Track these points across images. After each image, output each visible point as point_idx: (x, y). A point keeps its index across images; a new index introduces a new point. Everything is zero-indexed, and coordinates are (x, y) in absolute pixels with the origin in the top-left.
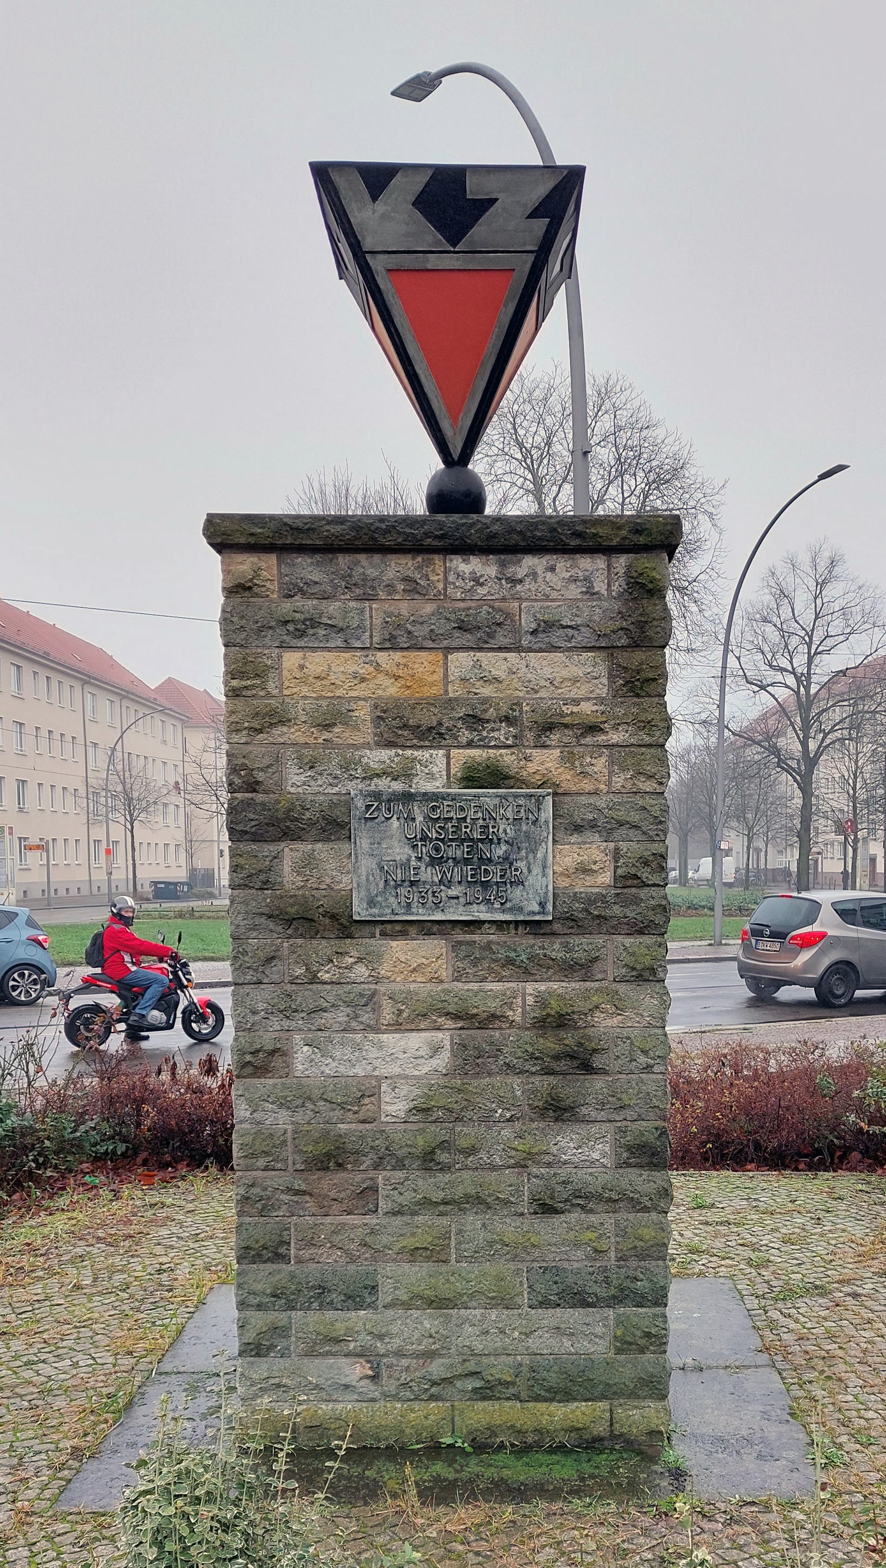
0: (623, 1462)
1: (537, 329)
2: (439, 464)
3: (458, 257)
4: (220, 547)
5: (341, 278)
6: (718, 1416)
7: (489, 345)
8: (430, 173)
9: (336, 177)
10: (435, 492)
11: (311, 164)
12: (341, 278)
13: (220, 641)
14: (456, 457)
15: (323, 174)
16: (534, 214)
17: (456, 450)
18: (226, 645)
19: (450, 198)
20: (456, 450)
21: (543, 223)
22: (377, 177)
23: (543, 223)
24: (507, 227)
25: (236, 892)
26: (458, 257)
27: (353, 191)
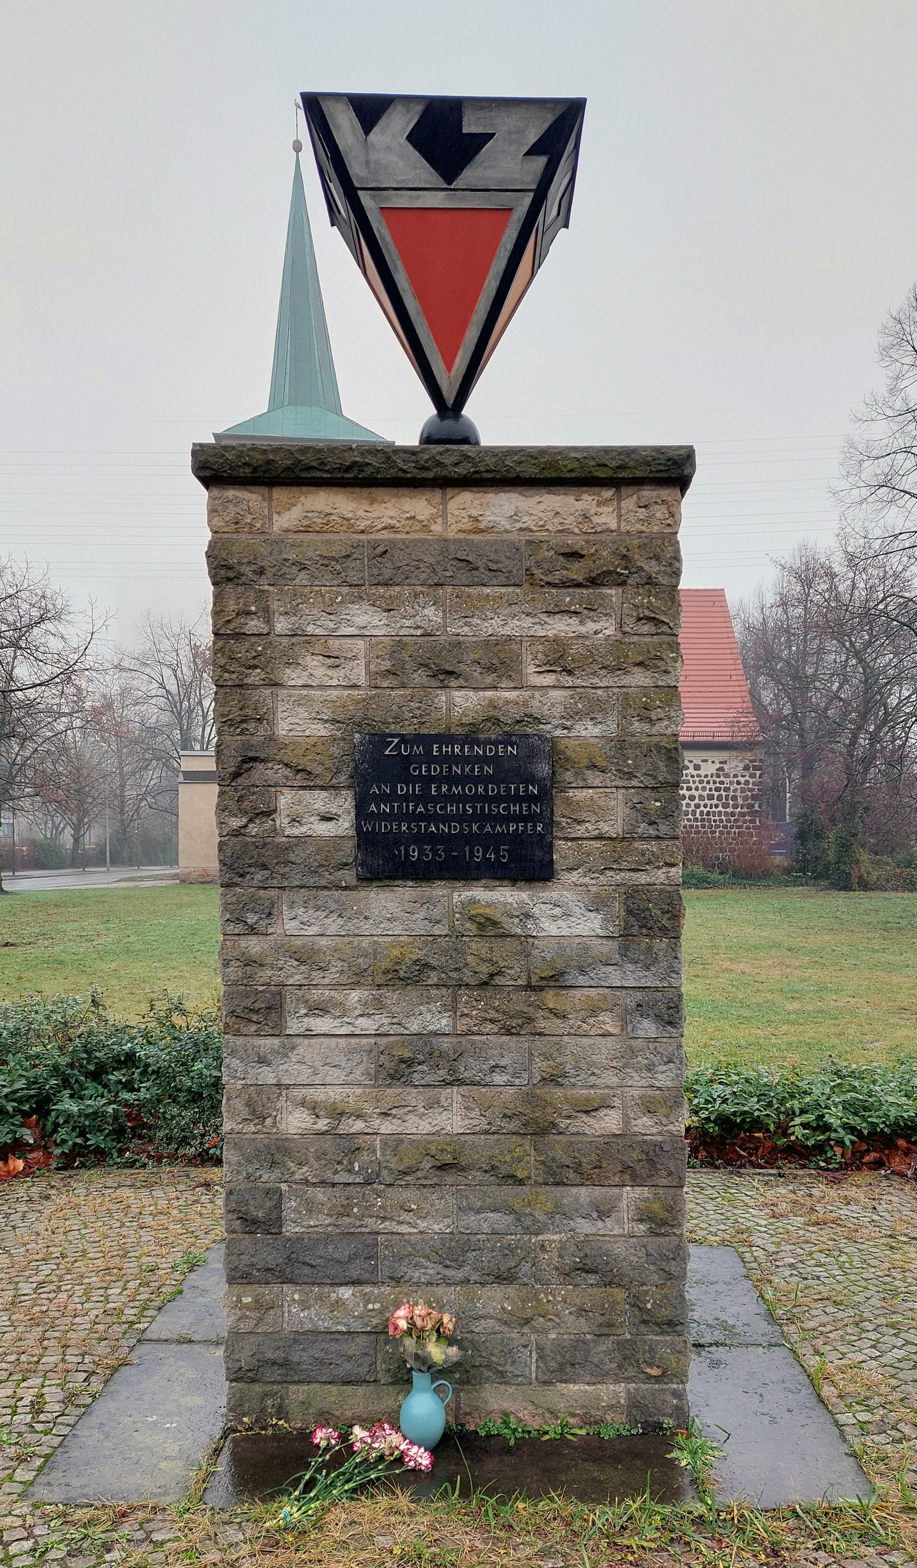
0: (643, 1456)
1: (533, 275)
2: (430, 410)
3: (449, 194)
4: (207, 482)
5: (333, 225)
6: (751, 1435)
7: (389, 238)
8: (419, 108)
9: (329, 108)
10: (425, 435)
11: (301, 94)
12: (333, 225)
13: (208, 581)
14: (449, 407)
15: (314, 106)
16: (533, 151)
17: (449, 395)
18: (214, 584)
19: (445, 132)
20: (449, 395)
21: (541, 161)
22: (370, 109)
23: (541, 161)
24: (504, 164)
25: (234, 1384)
26: (449, 194)
27: (345, 125)
